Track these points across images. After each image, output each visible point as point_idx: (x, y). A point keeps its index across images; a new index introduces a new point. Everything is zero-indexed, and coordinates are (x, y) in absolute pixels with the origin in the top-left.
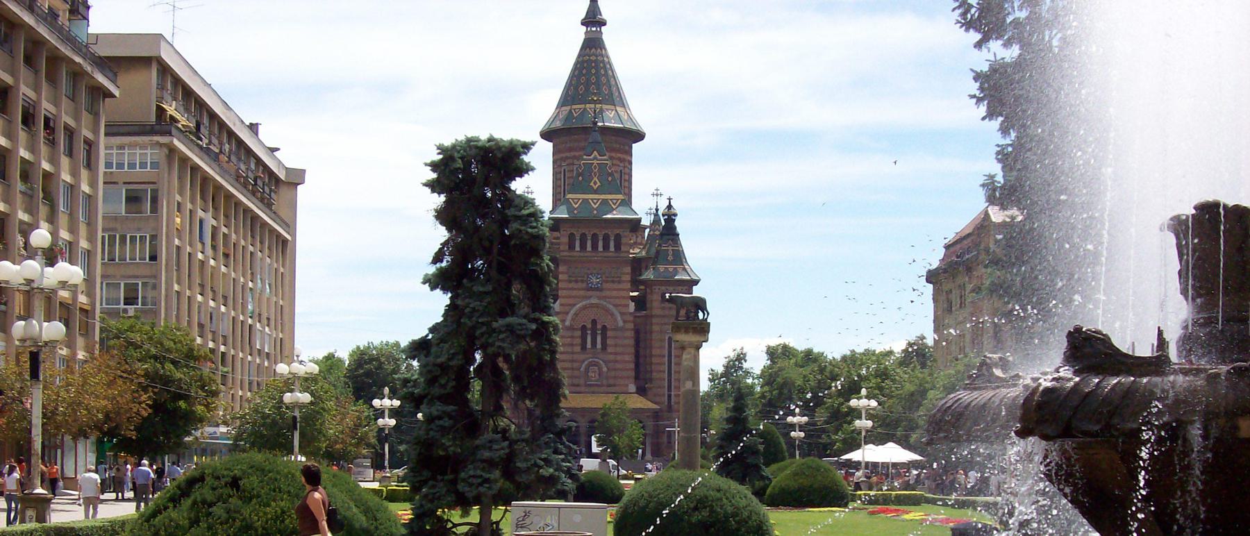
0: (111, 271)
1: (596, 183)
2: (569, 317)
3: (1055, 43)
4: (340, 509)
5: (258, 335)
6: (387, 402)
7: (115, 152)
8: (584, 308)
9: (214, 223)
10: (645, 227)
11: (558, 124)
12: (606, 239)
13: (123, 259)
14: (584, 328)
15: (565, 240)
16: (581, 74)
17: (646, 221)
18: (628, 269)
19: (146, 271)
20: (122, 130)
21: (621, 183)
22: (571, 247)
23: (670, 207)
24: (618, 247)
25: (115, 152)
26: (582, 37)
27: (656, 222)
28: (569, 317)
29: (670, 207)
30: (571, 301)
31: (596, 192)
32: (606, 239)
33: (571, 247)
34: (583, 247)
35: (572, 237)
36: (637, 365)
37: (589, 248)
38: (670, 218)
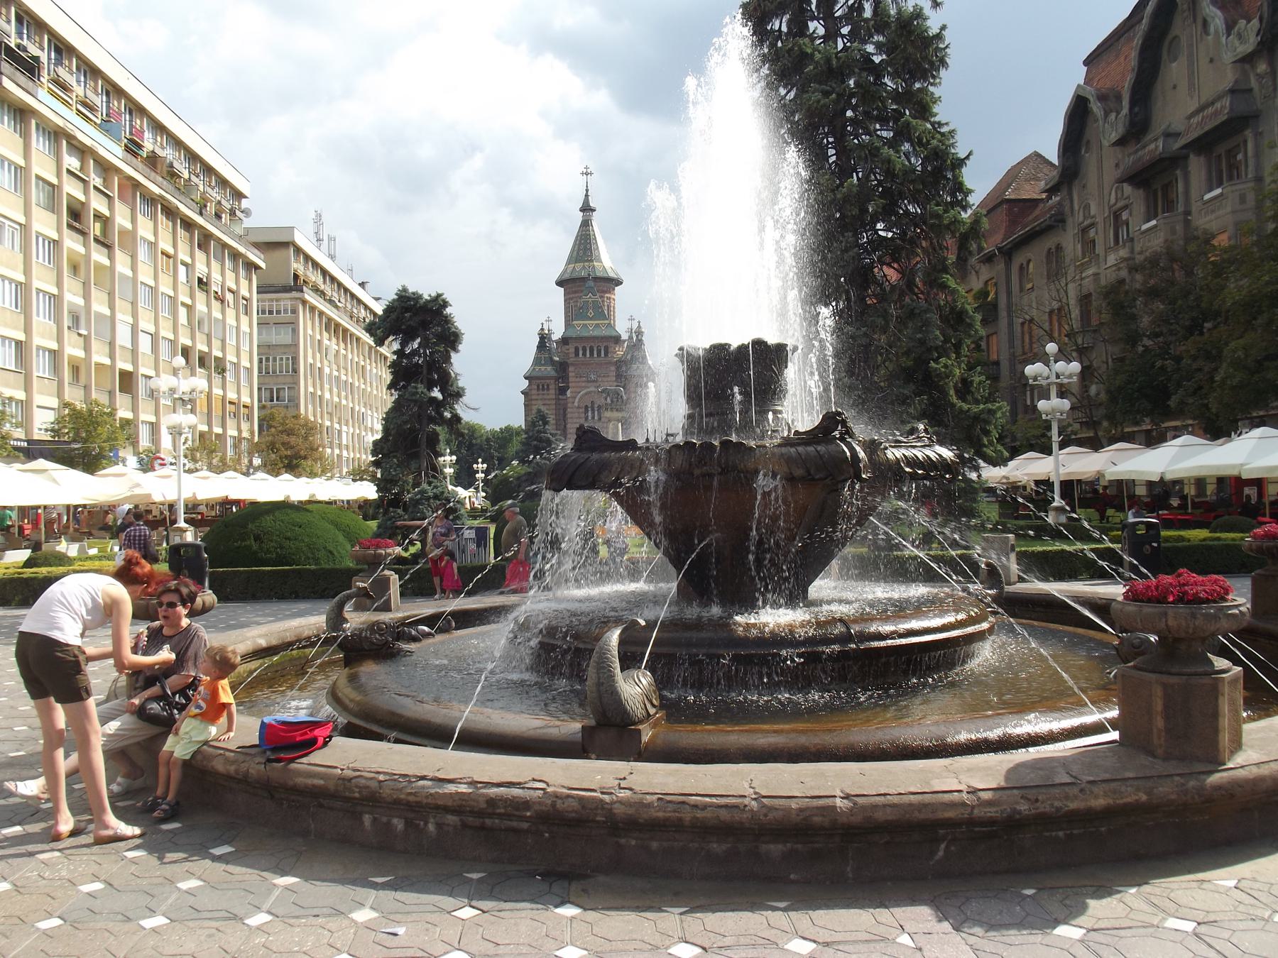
0: (267, 380)
1: (591, 313)
2: (577, 400)
3: (803, 214)
4: (141, 382)
5: (369, 418)
6: (448, 458)
7: (275, 303)
8: (586, 394)
9: (337, 348)
10: (624, 341)
11: (567, 276)
12: (584, 350)
13: (274, 372)
14: (586, 407)
15: (572, 350)
16: (581, 239)
17: (625, 336)
18: (613, 368)
19: (289, 380)
20: (267, 289)
21: (603, 313)
22: (577, 354)
23: (639, 327)
24: (606, 354)
25: (275, 303)
26: (580, 220)
27: (630, 338)
28: (577, 400)
29: (639, 327)
30: (578, 390)
31: (591, 319)
32: (584, 350)
33: (577, 354)
34: (584, 354)
35: (577, 350)
36: (565, 415)
37: (588, 355)
38: (639, 333)
